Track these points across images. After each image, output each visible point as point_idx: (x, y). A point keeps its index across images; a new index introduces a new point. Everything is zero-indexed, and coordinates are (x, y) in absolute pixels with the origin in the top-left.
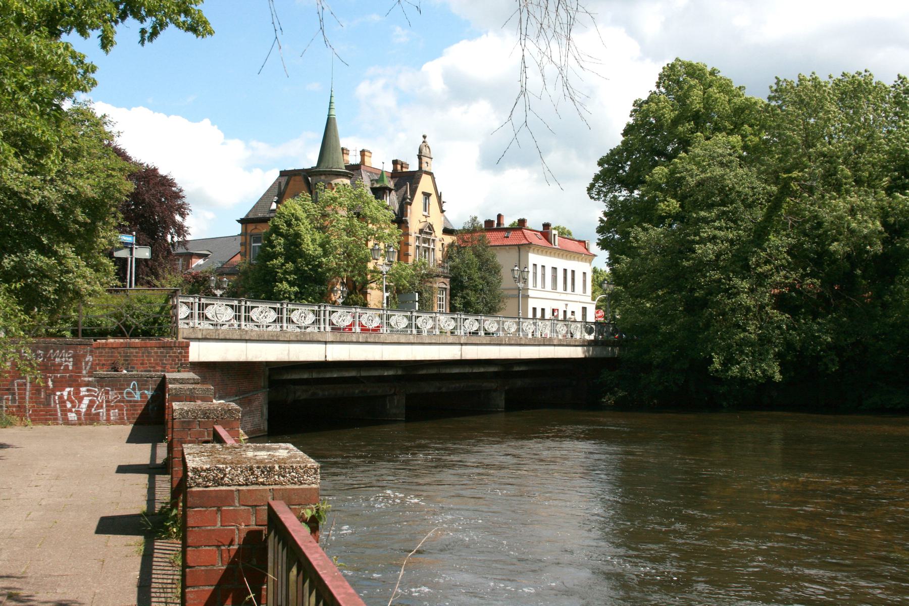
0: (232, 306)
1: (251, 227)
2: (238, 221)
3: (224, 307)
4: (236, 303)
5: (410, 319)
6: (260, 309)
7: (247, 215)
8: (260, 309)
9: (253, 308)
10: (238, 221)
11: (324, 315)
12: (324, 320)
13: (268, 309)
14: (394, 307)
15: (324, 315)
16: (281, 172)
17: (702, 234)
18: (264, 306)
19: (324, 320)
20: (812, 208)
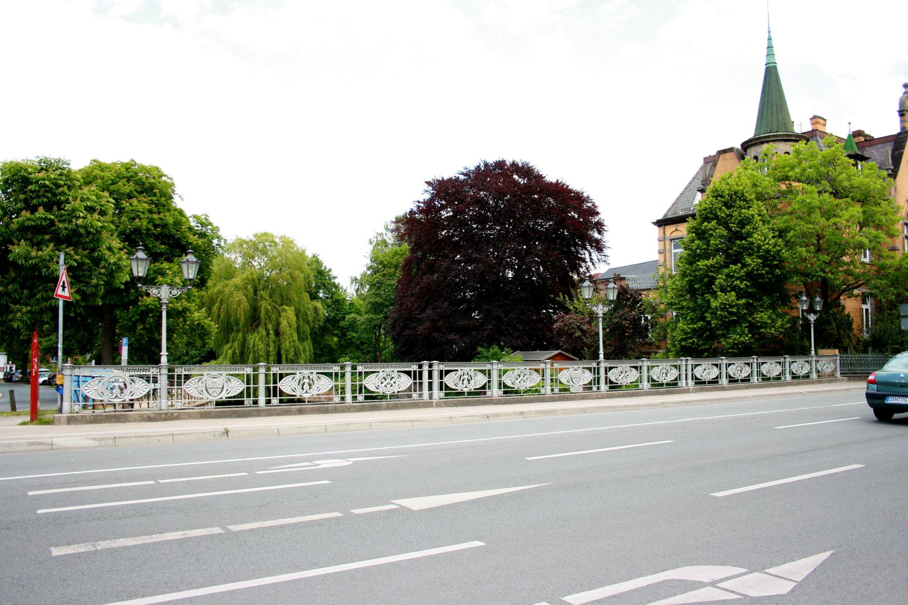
0: (590, 369)
1: (670, 229)
2: (653, 223)
3: (580, 371)
4: (414, 367)
5: (596, 371)
6: (620, 369)
7: (665, 216)
8: (620, 369)
9: (367, 374)
10: (655, 224)
11: (430, 377)
12: (430, 384)
13: (710, 366)
14: (135, 358)
15: (430, 377)
16: (705, 159)
17: (725, 233)
18: (624, 366)
19: (430, 384)
20: (111, 212)
